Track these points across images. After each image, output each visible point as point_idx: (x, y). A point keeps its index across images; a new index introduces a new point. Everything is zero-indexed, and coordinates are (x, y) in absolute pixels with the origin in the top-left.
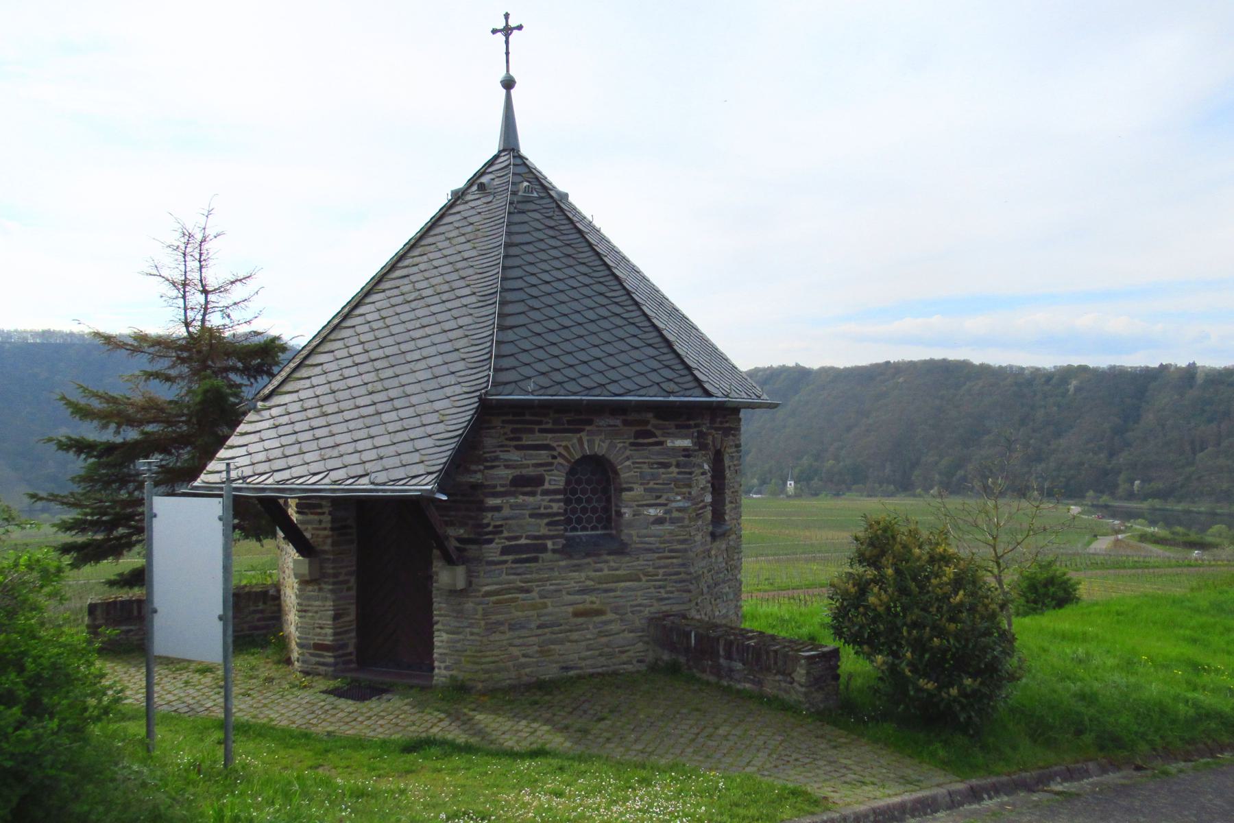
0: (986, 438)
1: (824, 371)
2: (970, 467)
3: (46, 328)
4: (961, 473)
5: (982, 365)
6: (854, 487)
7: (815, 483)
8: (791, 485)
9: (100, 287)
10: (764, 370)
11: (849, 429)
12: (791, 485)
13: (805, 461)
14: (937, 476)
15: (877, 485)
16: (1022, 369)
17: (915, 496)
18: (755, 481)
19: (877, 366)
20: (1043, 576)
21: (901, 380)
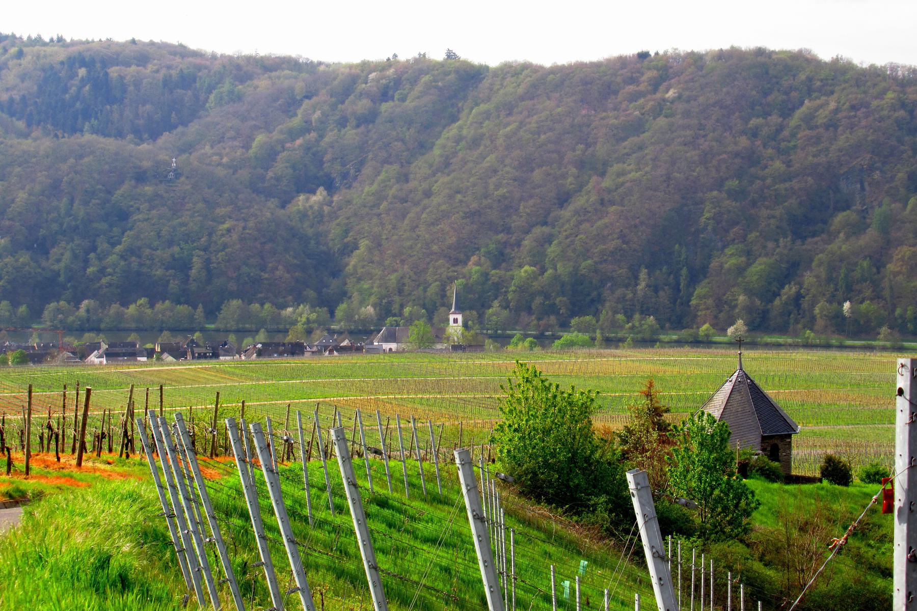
0: (840, 218)
1: (512, 72)
2: (809, 279)
3: (640, 51)
4: (789, 290)
5: (836, 61)
6: (574, 321)
7: (495, 311)
8: (455, 324)
9: (6, 31)
10: (382, 67)
11: (563, 199)
12: (455, 324)
13: (473, 268)
14: (742, 298)
15: (620, 317)
16: (626, 57)
17: (697, 342)
18: (370, 310)
19: (622, 62)
20: (873, 470)
21: (671, 94)
